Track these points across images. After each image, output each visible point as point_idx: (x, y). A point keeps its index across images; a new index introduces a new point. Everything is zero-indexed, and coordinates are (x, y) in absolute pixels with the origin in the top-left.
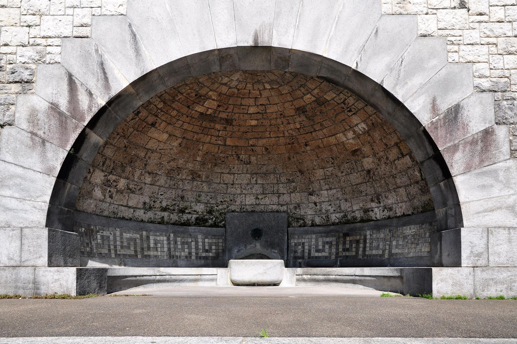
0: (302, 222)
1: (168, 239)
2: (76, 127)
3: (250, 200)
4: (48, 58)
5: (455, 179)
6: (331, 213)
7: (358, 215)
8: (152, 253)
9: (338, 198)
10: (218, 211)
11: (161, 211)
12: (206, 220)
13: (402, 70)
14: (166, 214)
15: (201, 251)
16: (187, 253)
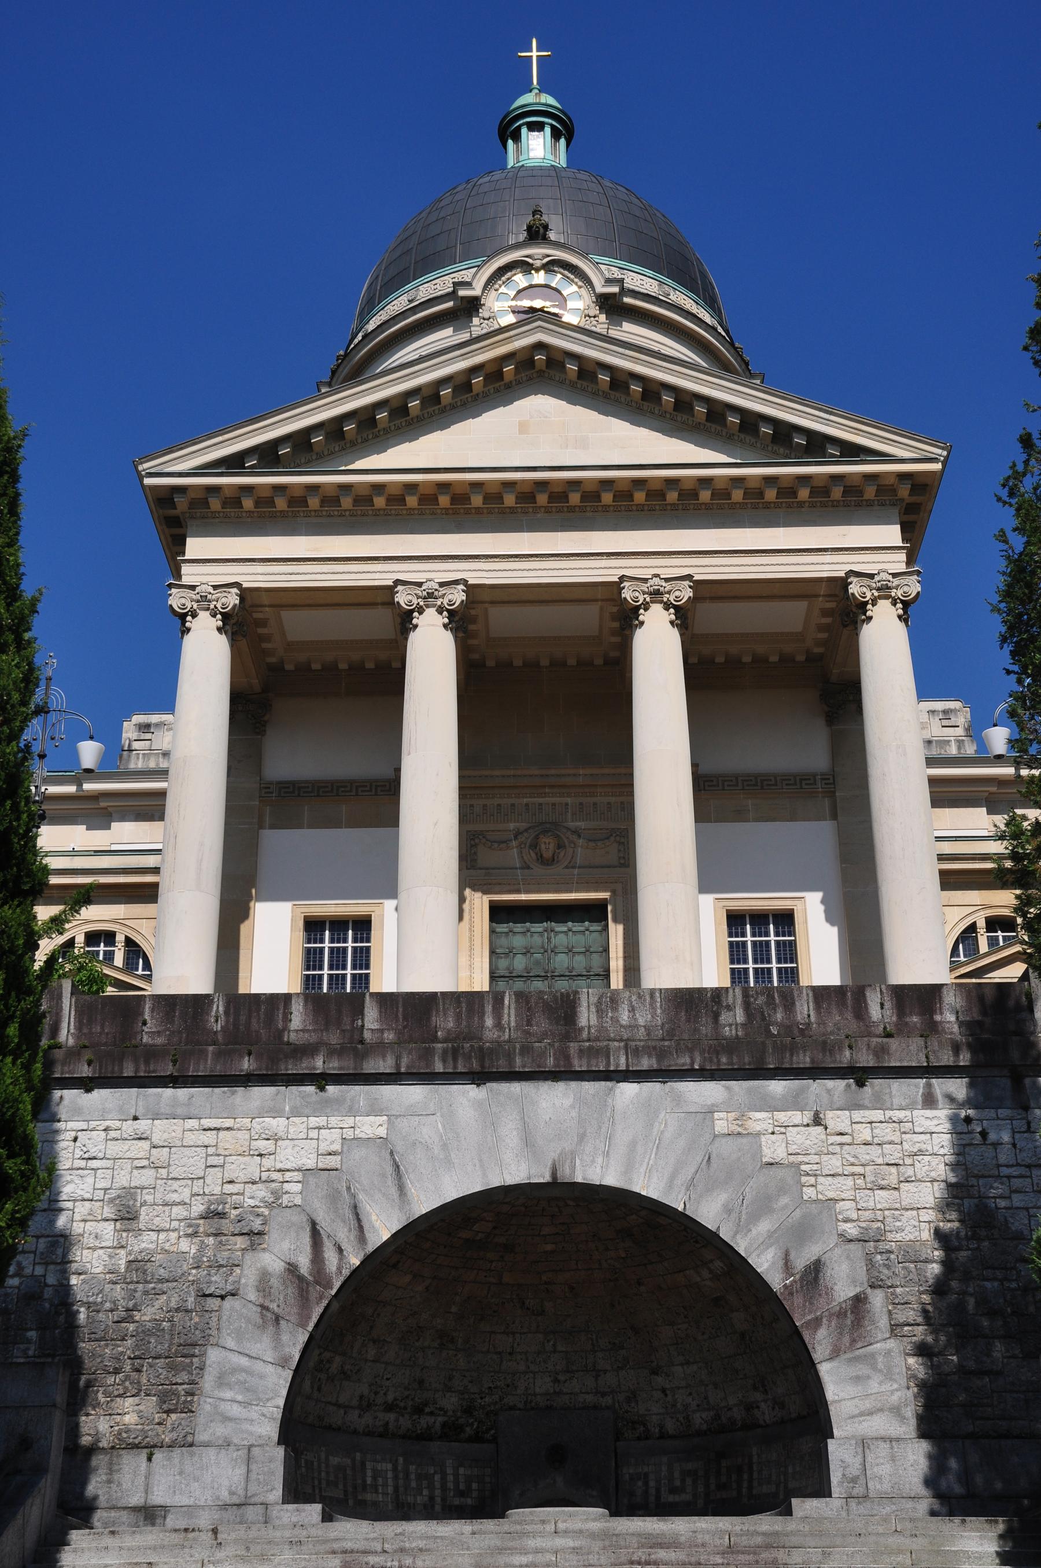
0: (642, 1429)
1: (395, 1469)
2: (321, 1298)
3: (542, 1385)
4: (285, 1200)
5: (818, 1366)
8: (369, 1497)
13: (744, 1212)
14: (391, 1416)
15: (452, 1494)
16: (426, 1499)
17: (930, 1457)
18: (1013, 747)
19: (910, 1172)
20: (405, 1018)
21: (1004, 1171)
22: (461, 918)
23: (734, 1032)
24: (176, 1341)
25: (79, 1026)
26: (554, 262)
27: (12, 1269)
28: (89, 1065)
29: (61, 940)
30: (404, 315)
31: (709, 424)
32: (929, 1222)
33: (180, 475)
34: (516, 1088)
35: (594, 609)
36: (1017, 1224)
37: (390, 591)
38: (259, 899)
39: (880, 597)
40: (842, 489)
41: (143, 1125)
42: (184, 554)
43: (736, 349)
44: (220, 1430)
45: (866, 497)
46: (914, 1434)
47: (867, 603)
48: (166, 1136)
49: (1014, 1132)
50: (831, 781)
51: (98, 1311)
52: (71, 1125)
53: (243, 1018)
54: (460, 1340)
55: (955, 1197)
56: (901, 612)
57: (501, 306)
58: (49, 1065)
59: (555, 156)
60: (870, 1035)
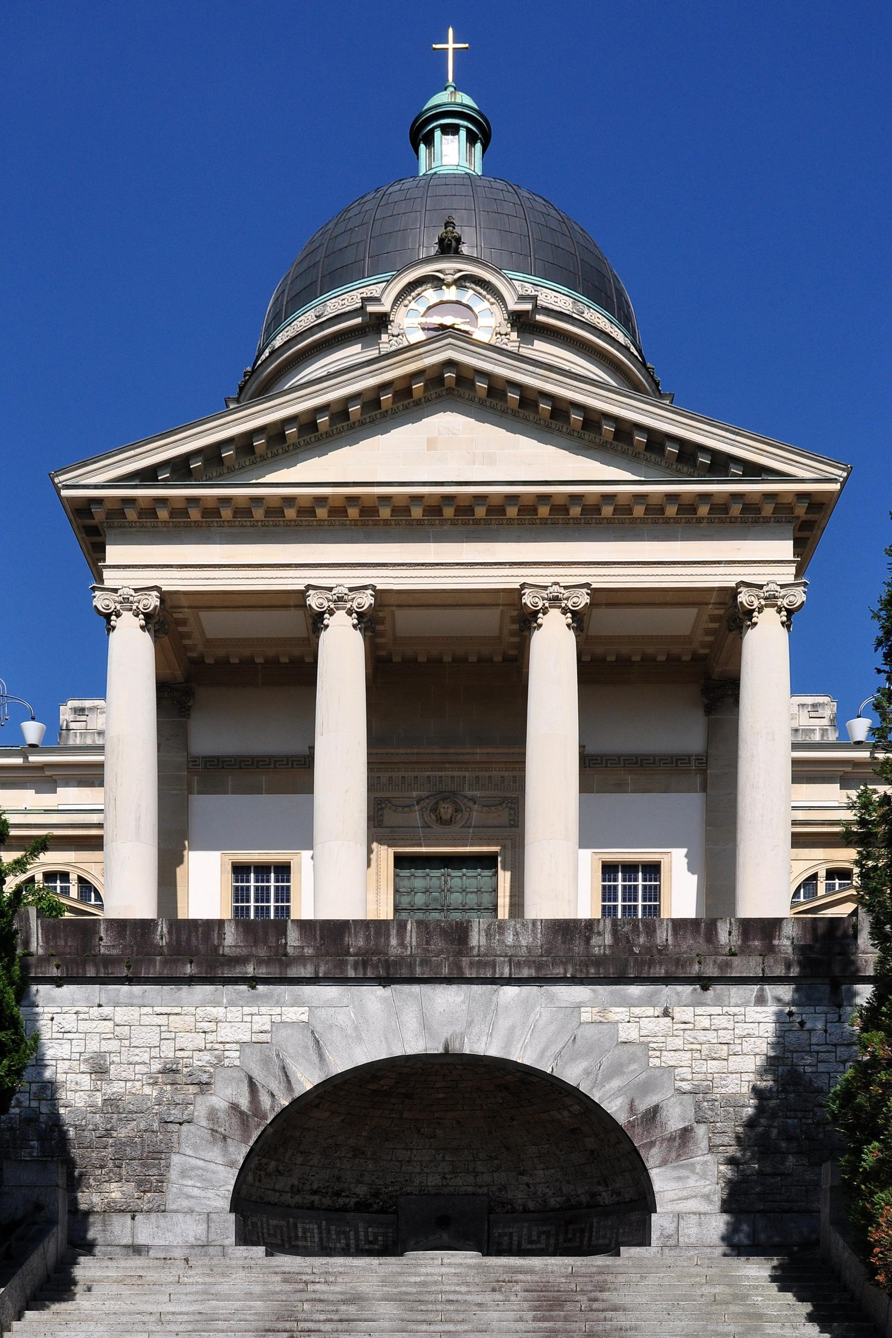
1: (320, 1228)
2: (259, 1125)
3: (433, 1181)
4: (226, 1062)
5: (650, 1171)
6: (550, 1197)
7: (584, 1199)
8: (300, 1243)
9: (557, 1180)
10: (387, 1193)
11: (311, 1194)
12: (370, 1205)
17: (728, 1224)
18: (874, 734)
19: (738, 1048)
20: (322, 938)
21: (816, 1048)
22: (369, 865)
23: (602, 951)
24: (146, 1149)
25: (47, 940)
26: (465, 278)
27: (13, 1103)
28: (58, 968)
29: (23, 877)
30: (311, 330)
31: (616, 443)
32: (749, 1081)
33: (96, 487)
34: (416, 988)
35: (496, 613)
36: (819, 1082)
37: (302, 594)
38: (191, 849)
39: (766, 606)
40: (741, 506)
41: (106, 1011)
42: (104, 560)
43: (647, 369)
44: (185, 1204)
45: (764, 514)
46: (718, 1211)
47: (753, 610)
48: (126, 1018)
49: (827, 1022)
50: (704, 761)
51: (84, 1130)
52: (46, 1009)
53: (184, 937)
54: (369, 1154)
55: (772, 1065)
56: (784, 619)
57: (410, 323)
58: (25, 968)
59: (470, 163)
60: (717, 954)
